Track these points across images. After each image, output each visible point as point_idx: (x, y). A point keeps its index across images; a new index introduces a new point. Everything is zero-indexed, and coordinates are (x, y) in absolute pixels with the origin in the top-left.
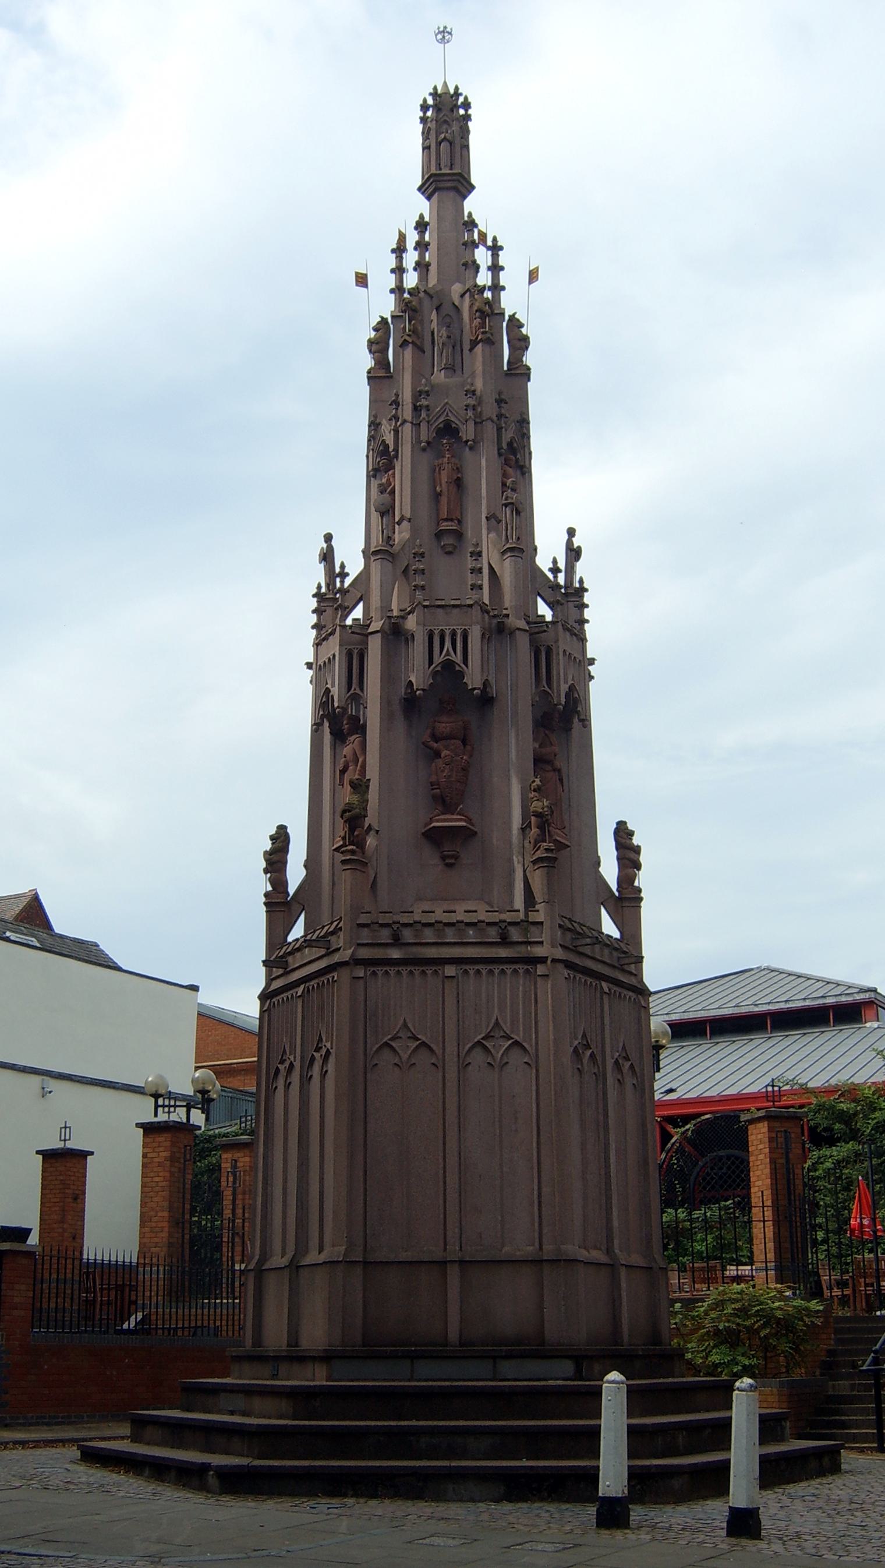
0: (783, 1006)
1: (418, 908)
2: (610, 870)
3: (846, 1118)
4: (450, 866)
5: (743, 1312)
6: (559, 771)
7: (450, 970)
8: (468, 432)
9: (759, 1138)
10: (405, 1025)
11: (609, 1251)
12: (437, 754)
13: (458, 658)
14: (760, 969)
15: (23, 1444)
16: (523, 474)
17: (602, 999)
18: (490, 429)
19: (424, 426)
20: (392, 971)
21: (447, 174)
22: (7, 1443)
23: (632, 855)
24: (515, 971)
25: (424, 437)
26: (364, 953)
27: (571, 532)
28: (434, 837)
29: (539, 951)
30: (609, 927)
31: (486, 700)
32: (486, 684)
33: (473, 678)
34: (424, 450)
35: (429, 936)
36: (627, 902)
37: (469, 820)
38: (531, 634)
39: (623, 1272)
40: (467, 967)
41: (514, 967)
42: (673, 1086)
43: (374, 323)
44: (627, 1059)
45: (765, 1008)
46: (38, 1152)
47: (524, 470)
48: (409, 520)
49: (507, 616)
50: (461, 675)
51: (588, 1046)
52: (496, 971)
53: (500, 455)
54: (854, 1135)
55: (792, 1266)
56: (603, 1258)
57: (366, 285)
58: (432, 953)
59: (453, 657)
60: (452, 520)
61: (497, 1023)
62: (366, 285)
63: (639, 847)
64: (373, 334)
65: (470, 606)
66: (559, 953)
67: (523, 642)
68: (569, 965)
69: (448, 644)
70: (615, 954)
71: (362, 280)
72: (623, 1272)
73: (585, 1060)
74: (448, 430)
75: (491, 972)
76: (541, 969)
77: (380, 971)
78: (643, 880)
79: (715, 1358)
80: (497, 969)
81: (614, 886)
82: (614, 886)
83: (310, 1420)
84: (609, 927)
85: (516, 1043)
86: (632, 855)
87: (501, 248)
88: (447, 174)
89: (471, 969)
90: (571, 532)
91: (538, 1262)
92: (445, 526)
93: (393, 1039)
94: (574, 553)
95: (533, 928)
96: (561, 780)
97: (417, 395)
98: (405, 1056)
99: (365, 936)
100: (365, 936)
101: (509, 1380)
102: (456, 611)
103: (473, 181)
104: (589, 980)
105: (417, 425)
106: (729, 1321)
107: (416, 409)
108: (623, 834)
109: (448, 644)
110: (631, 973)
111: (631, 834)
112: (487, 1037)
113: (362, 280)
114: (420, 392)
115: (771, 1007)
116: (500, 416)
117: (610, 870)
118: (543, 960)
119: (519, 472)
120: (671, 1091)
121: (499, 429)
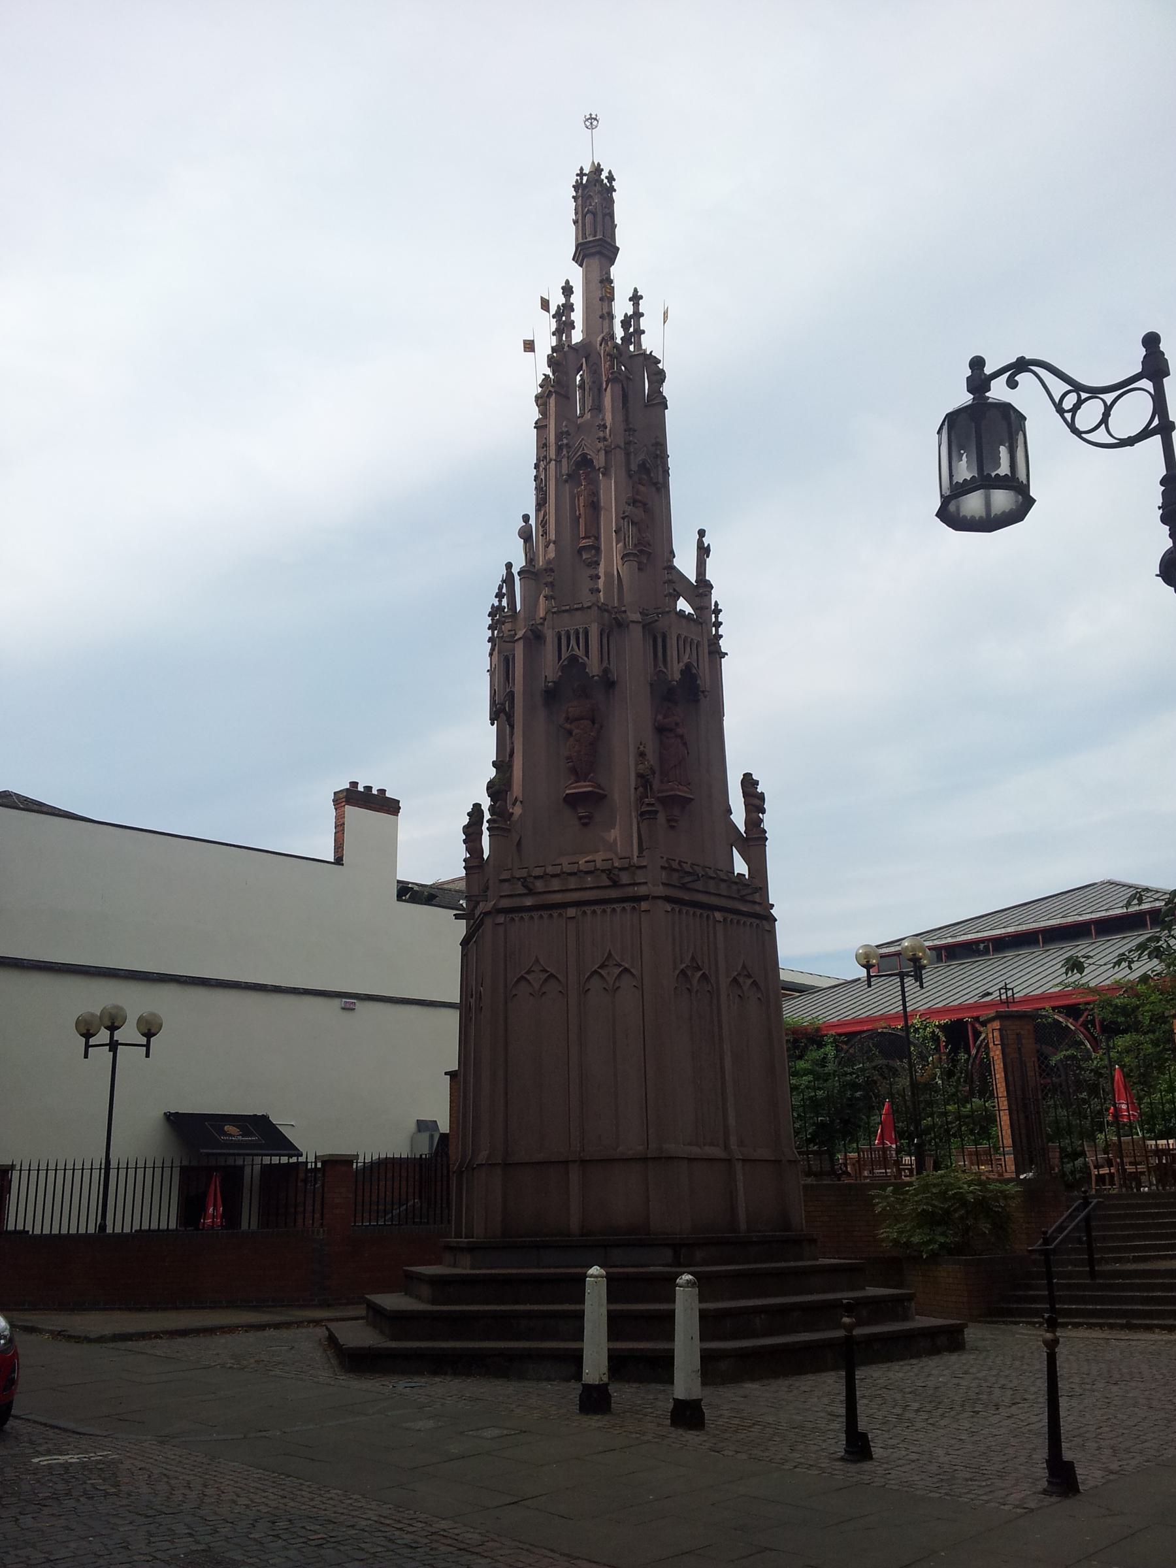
0: (1103, 914)
1: (564, 861)
2: (739, 817)
3: (1124, 1010)
4: (585, 825)
5: (943, 1196)
6: (682, 737)
7: (571, 912)
8: (600, 461)
9: (992, 1034)
10: (537, 961)
11: (726, 1147)
12: (570, 733)
13: (580, 653)
14: (1103, 883)
15: (277, 1326)
16: (658, 490)
17: (714, 928)
18: (619, 457)
19: (565, 461)
20: (526, 915)
21: (596, 244)
22: (302, 1322)
23: (756, 802)
24: (604, 911)
25: (565, 471)
26: (506, 903)
27: (702, 533)
28: (572, 801)
29: (642, 890)
30: (741, 867)
31: (609, 683)
32: (606, 671)
33: (594, 667)
34: (566, 481)
35: (556, 884)
36: (754, 841)
37: (599, 787)
38: (644, 627)
39: (739, 1166)
40: (585, 908)
41: (623, 905)
42: (990, 991)
43: (540, 382)
44: (749, 976)
45: (1088, 917)
46: (446, 1074)
47: (661, 486)
48: (554, 543)
49: (625, 612)
50: (584, 665)
51: (699, 969)
52: (609, 910)
53: (630, 476)
54: (1135, 1027)
55: (1026, 1155)
56: (717, 1152)
57: (533, 351)
58: (558, 898)
59: (577, 652)
60: (589, 538)
61: (610, 954)
62: (533, 351)
63: (762, 793)
64: (540, 390)
65: (589, 607)
66: (660, 891)
67: (636, 632)
68: (668, 899)
69: (573, 642)
70: (735, 887)
71: (529, 346)
72: (739, 1166)
73: (695, 981)
74: (585, 462)
75: (604, 911)
76: (644, 905)
77: (516, 916)
78: (769, 821)
79: (916, 1239)
80: (609, 908)
81: (742, 829)
82: (742, 829)
83: (488, 1304)
84: (741, 867)
85: (626, 970)
86: (756, 802)
87: (641, 297)
88: (596, 244)
89: (589, 910)
90: (702, 533)
91: (645, 1159)
92: (584, 543)
93: (528, 972)
94: (703, 551)
95: (639, 872)
96: (685, 744)
97: (559, 436)
98: (536, 986)
99: (506, 889)
100: (506, 889)
101: (616, 1266)
102: (578, 613)
103: (618, 245)
104: (699, 912)
105: (558, 462)
106: (927, 1204)
107: (559, 449)
108: (749, 783)
109: (573, 642)
110: (755, 902)
111: (757, 783)
112: (602, 966)
113: (529, 346)
114: (562, 433)
115: (1093, 916)
116: (628, 443)
117: (739, 817)
118: (645, 898)
119: (654, 489)
120: (989, 994)
121: (628, 454)
